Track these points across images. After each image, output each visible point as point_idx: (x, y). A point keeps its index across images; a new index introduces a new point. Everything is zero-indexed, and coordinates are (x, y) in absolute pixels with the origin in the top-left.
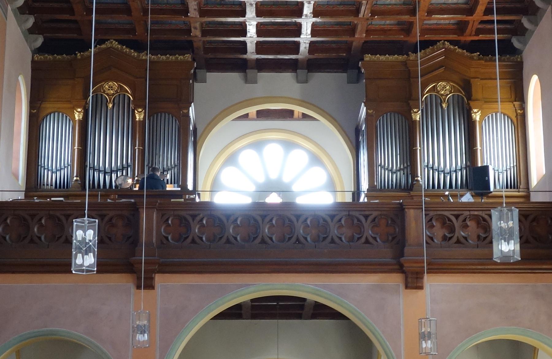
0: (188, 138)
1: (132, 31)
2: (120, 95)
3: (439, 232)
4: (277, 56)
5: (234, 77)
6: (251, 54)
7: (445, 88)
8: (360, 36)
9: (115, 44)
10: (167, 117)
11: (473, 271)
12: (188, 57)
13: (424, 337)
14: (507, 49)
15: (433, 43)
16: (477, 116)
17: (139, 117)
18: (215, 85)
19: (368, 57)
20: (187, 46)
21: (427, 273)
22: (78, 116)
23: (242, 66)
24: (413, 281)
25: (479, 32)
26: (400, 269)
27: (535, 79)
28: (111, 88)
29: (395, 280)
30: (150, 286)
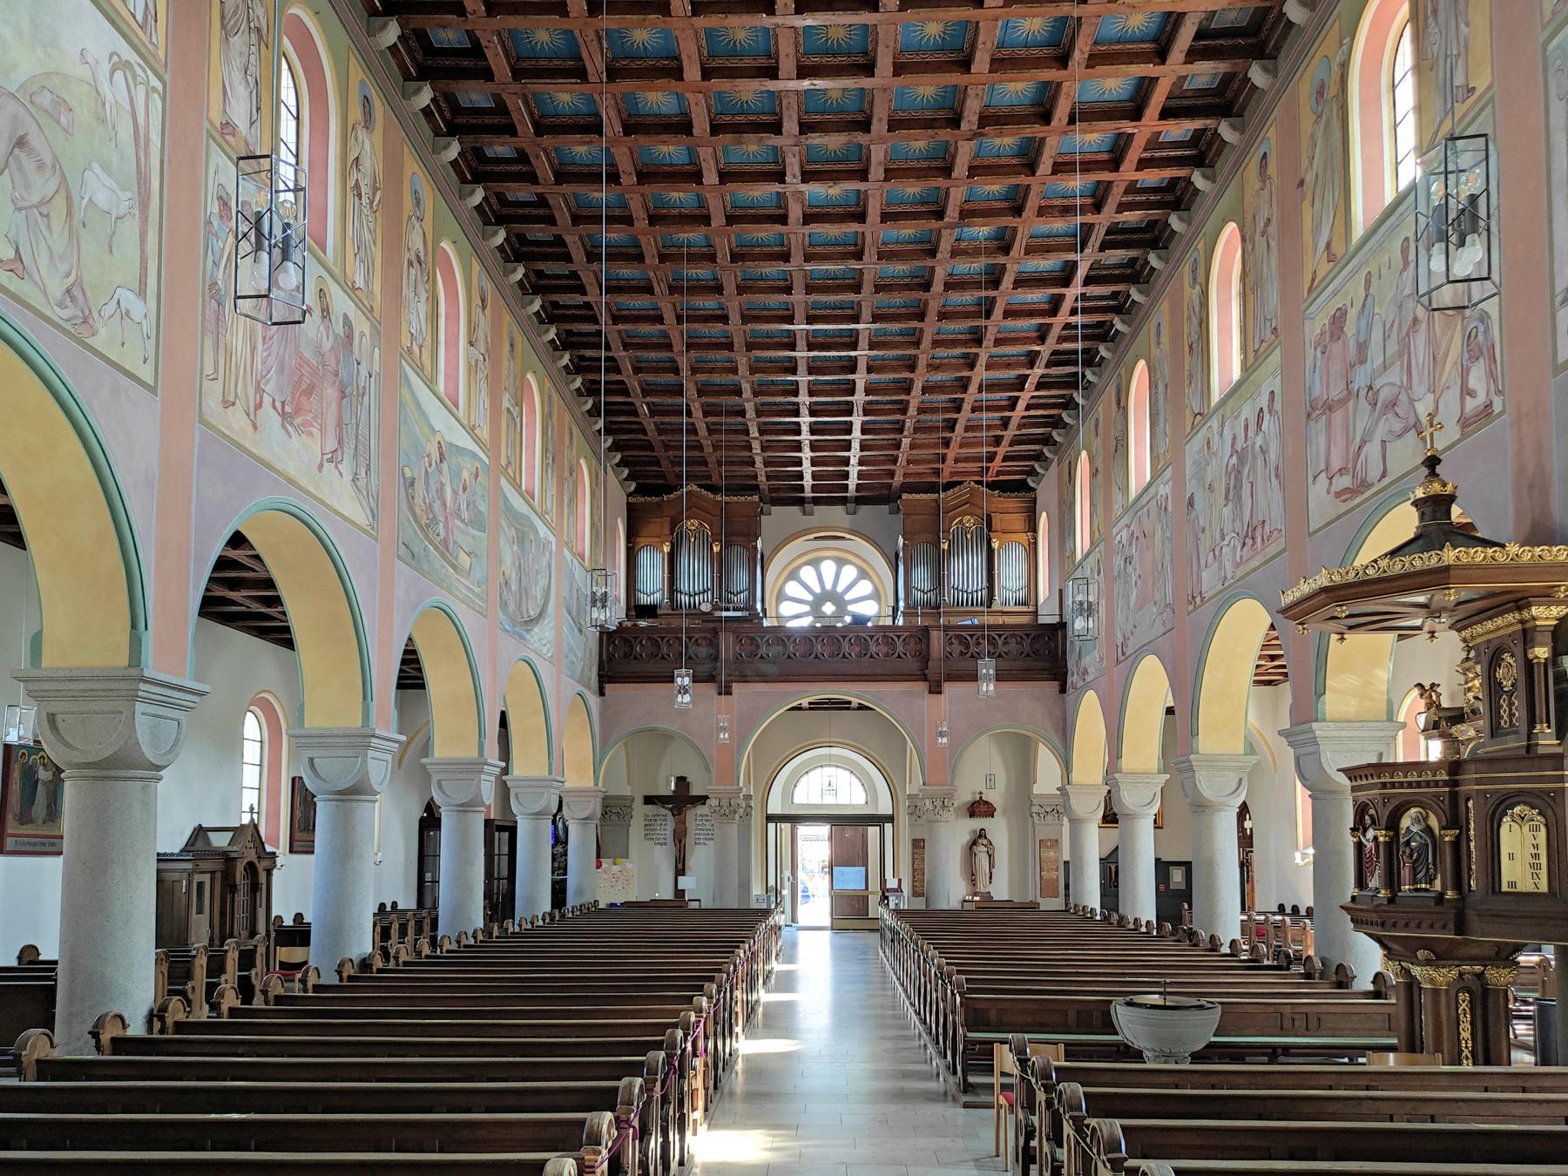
0: (757, 562)
1: (709, 477)
2: (699, 531)
3: (957, 648)
4: (831, 493)
5: (796, 509)
6: (808, 494)
7: (969, 521)
8: (898, 479)
9: (695, 488)
10: (738, 539)
11: (1204, 323)
12: (756, 498)
13: (941, 734)
14: (1022, 487)
15: (961, 483)
16: (995, 545)
17: (716, 549)
18: (778, 518)
19: (905, 496)
20: (755, 489)
21: (791, 962)
22: (666, 549)
23: (800, 502)
24: (936, 690)
25: (1061, 339)
26: (925, 678)
27: (1044, 514)
28: (691, 524)
29: (921, 687)
30: (729, 693)
